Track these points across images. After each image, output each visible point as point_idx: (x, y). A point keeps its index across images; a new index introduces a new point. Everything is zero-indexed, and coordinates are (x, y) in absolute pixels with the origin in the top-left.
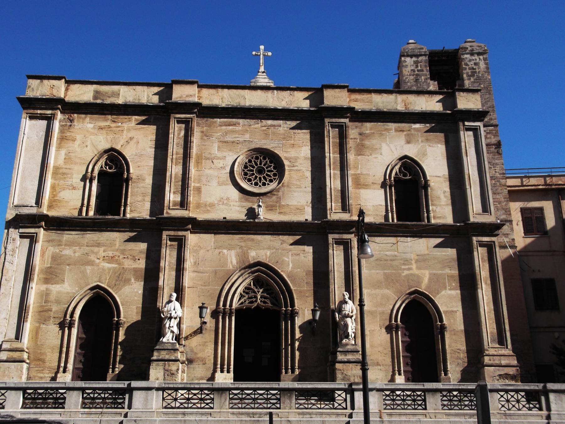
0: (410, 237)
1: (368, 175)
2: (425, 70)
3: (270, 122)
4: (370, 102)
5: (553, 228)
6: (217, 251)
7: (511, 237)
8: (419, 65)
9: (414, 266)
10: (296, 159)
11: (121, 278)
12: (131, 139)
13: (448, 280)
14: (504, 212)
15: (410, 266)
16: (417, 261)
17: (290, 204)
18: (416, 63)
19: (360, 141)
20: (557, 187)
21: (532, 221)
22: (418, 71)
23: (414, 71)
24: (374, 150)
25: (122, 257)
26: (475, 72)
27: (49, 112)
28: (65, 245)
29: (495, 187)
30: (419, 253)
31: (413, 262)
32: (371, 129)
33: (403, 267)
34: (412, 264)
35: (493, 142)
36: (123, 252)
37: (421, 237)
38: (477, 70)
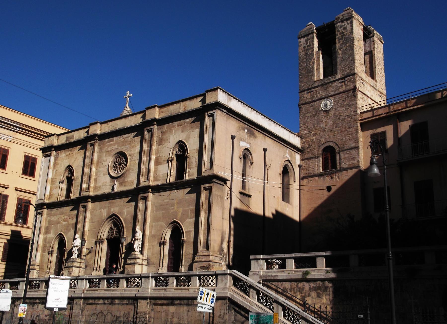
0: (176, 189)
1: (162, 156)
3: (126, 136)
4: (168, 111)
5: (392, 146)
7: (357, 159)
9: (176, 207)
10: (133, 154)
12: (76, 158)
14: (354, 141)
17: (129, 180)
18: (306, 41)
20: (394, 113)
21: (377, 143)
27: (50, 153)
31: (176, 204)
32: (167, 128)
33: (171, 208)
35: (351, 88)
36: (69, 216)
37: (181, 189)
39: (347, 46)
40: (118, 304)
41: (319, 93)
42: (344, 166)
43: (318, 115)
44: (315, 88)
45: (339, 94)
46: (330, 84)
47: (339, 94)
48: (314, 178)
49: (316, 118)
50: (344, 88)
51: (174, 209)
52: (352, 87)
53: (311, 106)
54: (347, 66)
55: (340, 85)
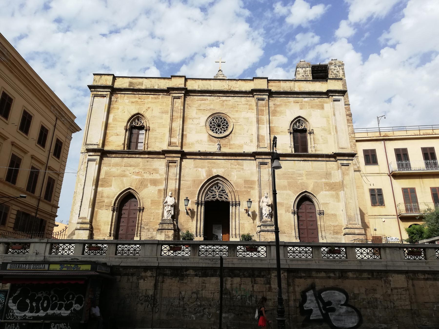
6: (195, 169)
9: (304, 178)
16: (306, 175)
17: (235, 143)
25: (143, 172)
28: (113, 166)
30: (307, 171)
32: (280, 102)
33: (298, 178)
40: (353, 278)
51: (302, 179)
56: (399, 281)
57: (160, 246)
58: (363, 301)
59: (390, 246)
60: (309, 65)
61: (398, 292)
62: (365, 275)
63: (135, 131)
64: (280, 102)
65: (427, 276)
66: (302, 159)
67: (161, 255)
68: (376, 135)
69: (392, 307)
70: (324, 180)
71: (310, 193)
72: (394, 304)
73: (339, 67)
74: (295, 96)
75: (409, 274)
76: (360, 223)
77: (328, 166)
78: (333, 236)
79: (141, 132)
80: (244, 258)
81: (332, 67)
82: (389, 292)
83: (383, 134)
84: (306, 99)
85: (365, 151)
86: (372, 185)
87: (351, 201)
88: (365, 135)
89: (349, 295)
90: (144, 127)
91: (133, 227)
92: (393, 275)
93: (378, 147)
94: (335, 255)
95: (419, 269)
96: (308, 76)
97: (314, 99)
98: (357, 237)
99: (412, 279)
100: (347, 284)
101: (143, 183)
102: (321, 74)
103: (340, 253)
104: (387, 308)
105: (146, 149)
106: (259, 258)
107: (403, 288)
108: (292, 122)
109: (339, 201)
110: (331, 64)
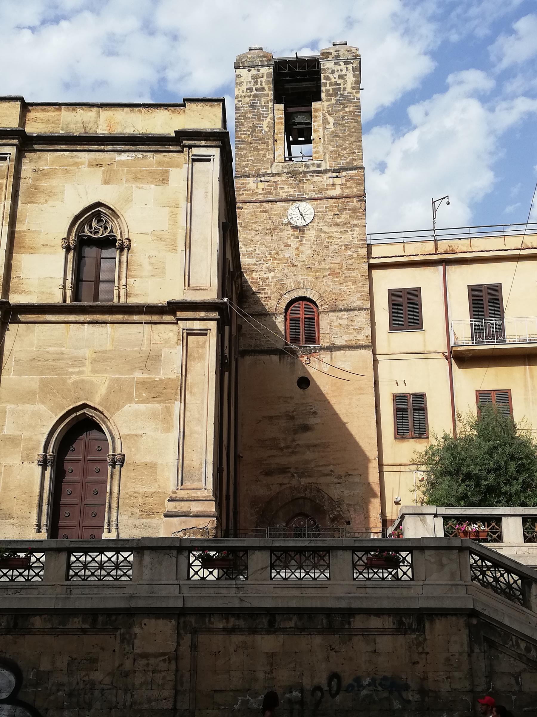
2: (266, 88)
8: (259, 80)
9: (87, 369)
11: (120, 392)
13: (137, 388)
14: (359, 295)
15: (81, 369)
16: (94, 361)
18: (255, 78)
19: (33, 181)
22: (257, 90)
23: (251, 90)
24: (51, 194)
26: (339, 89)
29: (350, 259)
30: (97, 349)
32: (52, 163)
33: (70, 370)
34: (84, 365)
35: (353, 194)
38: (342, 86)
39: (346, 112)
40: (43, 632)
41: (282, 188)
42: (338, 342)
43: (278, 230)
44: (274, 175)
45: (326, 198)
46: (308, 175)
47: (326, 198)
48: (268, 357)
49: (274, 238)
50: (337, 191)
51: (80, 373)
52: (355, 190)
53: (263, 211)
54: (345, 149)
55: (330, 181)
56: (157, 636)
57: (64, 556)
58: (58, 690)
59: (155, 545)
60: (269, 60)
61: (147, 665)
62: (76, 623)
63: (90, 252)
64: (52, 163)
65: (232, 622)
66: (88, 318)
67: (189, 579)
68: (423, 250)
69: (128, 704)
70: (138, 375)
71: (95, 409)
72: (132, 695)
73: (345, 63)
74: (95, 147)
75: (188, 618)
76: (210, 486)
77: (156, 337)
78: (137, 523)
79: (106, 253)
80: (100, 583)
81: (327, 65)
82: (128, 665)
83: (443, 246)
84: (124, 157)
85: (393, 294)
86: (401, 384)
87: (198, 428)
88: (397, 250)
89: (24, 675)
90: (115, 240)
91: (96, 507)
92: (146, 621)
93: (427, 282)
94: (16, 573)
95: (214, 605)
96: (263, 89)
97: (144, 157)
98: (193, 522)
99: (194, 632)
100: (25, 649)
101: (120, 392)
102: (305, 84)
103: (27, 566)
104: (116, 707)
105: (122, 300)
106: (29, 585)
107: (164, 654)
108: (77, 218)
109: (168, 430)
110: (326, 55)
